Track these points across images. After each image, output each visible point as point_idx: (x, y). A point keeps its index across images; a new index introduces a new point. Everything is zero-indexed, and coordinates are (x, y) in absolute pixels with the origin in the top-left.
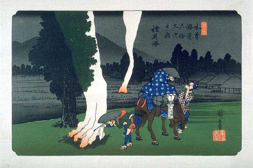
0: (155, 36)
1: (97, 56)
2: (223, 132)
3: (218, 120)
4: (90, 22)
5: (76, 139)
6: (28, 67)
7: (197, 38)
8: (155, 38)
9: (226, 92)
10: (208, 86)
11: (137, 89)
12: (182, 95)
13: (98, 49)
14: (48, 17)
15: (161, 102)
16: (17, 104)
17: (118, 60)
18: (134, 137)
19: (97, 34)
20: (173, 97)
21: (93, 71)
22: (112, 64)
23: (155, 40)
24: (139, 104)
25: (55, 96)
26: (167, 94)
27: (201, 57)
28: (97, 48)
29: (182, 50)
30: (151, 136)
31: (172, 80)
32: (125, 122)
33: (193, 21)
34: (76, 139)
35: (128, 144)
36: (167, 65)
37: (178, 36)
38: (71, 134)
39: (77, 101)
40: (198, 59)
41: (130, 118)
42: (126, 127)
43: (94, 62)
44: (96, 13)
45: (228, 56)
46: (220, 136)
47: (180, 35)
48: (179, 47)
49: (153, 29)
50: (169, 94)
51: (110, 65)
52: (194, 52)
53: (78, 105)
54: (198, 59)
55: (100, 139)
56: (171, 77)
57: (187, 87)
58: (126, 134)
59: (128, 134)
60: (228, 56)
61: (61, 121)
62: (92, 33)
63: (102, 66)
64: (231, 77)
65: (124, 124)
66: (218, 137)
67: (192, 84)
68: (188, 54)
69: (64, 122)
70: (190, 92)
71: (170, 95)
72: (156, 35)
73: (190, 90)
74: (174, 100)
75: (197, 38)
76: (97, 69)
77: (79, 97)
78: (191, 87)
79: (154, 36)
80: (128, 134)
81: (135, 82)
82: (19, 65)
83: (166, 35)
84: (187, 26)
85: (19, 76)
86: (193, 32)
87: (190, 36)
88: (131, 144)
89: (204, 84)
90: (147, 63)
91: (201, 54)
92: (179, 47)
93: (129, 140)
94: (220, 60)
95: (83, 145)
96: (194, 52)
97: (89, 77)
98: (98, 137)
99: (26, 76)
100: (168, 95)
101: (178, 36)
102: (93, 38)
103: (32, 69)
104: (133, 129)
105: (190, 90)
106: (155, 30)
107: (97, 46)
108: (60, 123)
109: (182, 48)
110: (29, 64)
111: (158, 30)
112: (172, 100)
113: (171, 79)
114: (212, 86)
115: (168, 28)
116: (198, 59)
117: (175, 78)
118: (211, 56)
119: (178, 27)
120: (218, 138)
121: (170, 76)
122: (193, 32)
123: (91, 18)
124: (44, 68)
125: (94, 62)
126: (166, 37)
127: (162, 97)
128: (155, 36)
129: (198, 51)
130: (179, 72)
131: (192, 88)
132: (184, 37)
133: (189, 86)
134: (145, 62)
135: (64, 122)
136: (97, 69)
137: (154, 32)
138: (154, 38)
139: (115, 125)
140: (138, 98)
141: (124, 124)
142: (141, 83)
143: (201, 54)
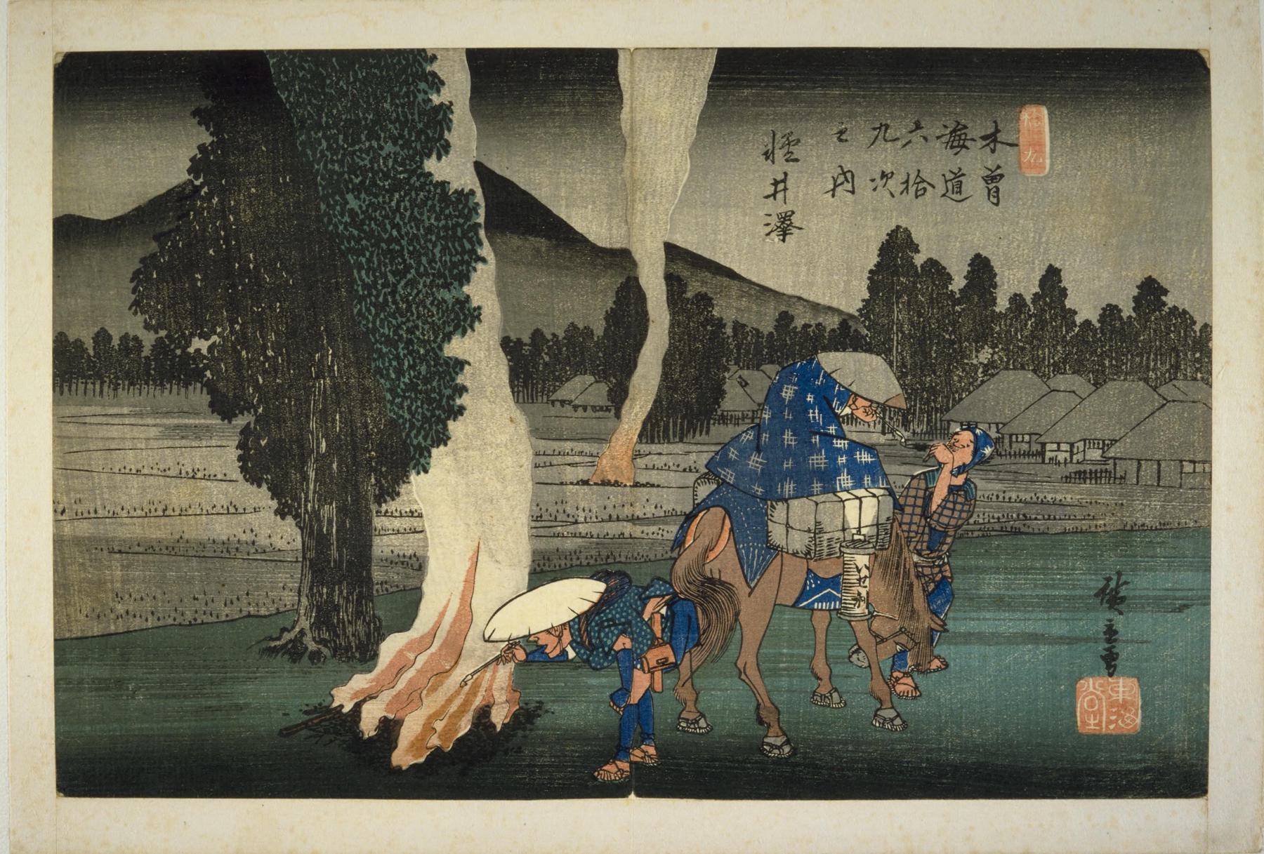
2: (1125, 688)
3: (1101, 626)
4: (446, 109)
5: (369, 724)
6: (130, 345)
8: (780, 196)
9: (1135, 464)
10: (1048, 447)
12: (910, 524)
14: (232, 88)
16: (78, 541)
20: (870, 506)
21: (460, 364)
22: (561, 335)
23: (779, 207)
27: (1017, 301)
28: (481, 244)
29: (919, 260)
34: (369, 724)
35: (637, 752)
36: (846, 337)
37: (894, 185)
38: (343, 698)
39: (378, 522)
40: (1002, 304)
44: (486, 64)
45: (1151, 291)
47: (907, 182)
48: (897, 247)
52: (981, 269)
53: (383, 546)
54: (1002, 304)
55: (494, 726)
60: (1151, 291)
63: (509, 346)
65: (617, 647)
68: (950, 278)
72: (784, 181)
74: (877, 525)
77: (392, 506)
78: (965, 456)
82: (84, 334)
85: (82, 387)
87: (956, 183)
91: (1016, 280)
95: (402, 757)
96: (981, 269)
98: (483, 714)
101: (894, 185)
102: (459, 193)
107: (482, 233)
110: (134, 325)
118: (1064, 293)
119: (897, 139)
120: (1101, 715)
123: (456, 88)
124: (210, 349)
125: (465, 317)
126: (839, 189)
127: (814, 507)
131: (968, 459)
132: (925, 189)
134: (730, 325)
136: (479, 354)
137: (773, 162)
141: (617, 647)
142: (707, 433)
143: (1016, 280)
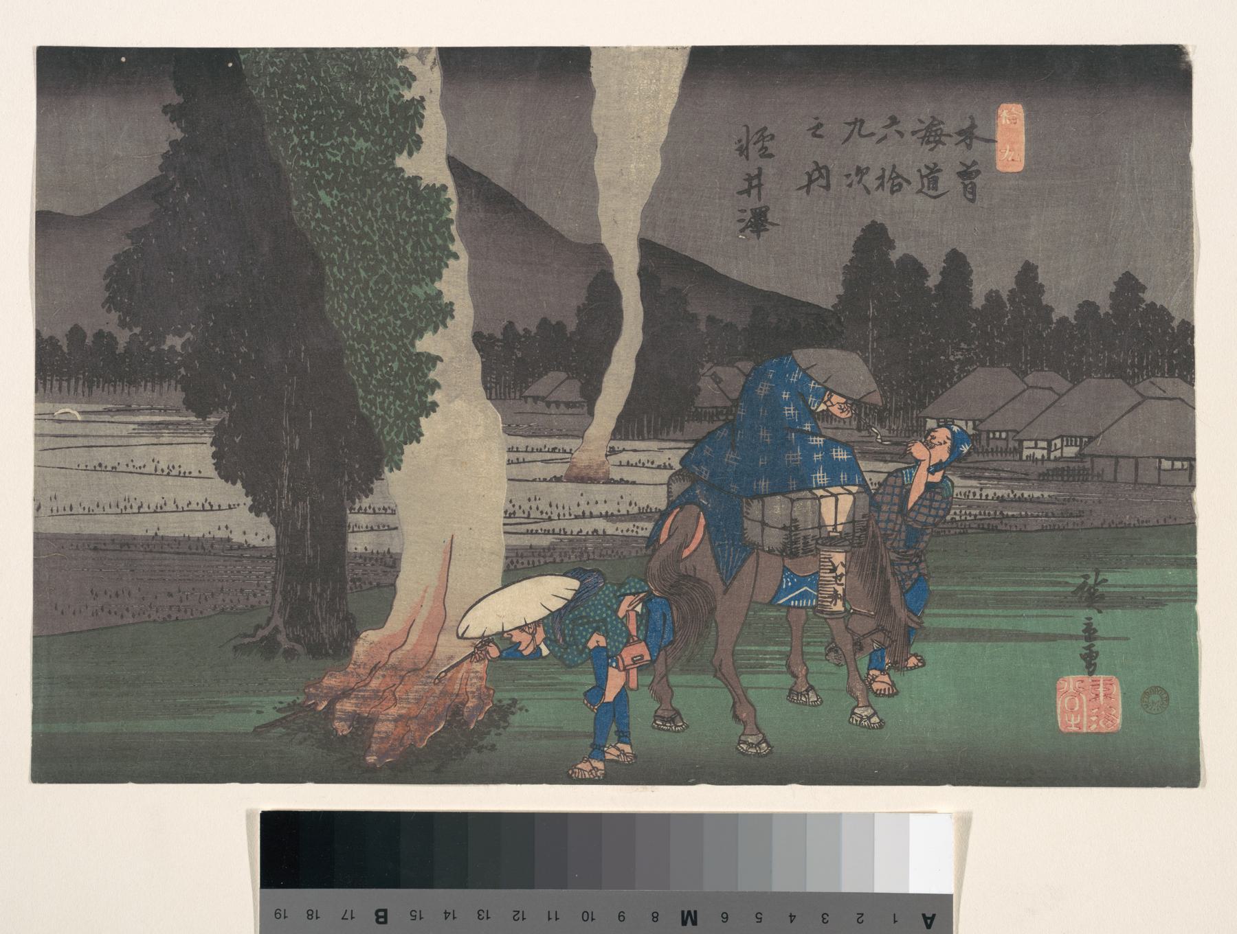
0: (754, 182)
1: (454, 284)
7: (971, 193)
8: (754, 192)
11: (661, 459)
13: (458, 246)
14: (203, 79)
15: (784, 528)
16: (56, 538)
17: (561, 301)
18: (642, 707)
19: (454, 165)
20: (846, 502)
23: (752, 202)
24: (670, 536)
25: (236, 493)
26: (817, 488)
28: (453, 240)
29: (895, 256)
30: (734, 706)
31: (843, 416)
32: (596, 637)
33: (952, 109)
41: (621, 614)
42: (602, 661)
43: (440, 313)
46: (1087, 706)
48: (874, 238)
49: (744, 142)
50: (823, 487)
51: (522, 333)
52: (957, 265)
53: (358, 543)
56: (836, 399)
57: (918, 450)
58: (604, 694)
59: (610, 696)
60: (1129, 286)
61: (268, 624)
62: (428, 164)
63: (479, 339)
64: (1145, 398)
66: (1081, 712)
67: (943, 434)
68: (85, 337)
69: (281, 628)
70: (932, 479)
71: (832, 495)
72: (759, 176)
73: (933, 470)
75: (971, 193)
76: (451, 348)
79: (749, 179)
80: (610, 696)
81: (649, 422)
83: (810, 175)
84: (919, 126)
86: (950, 155)
87: (932, 174)
88: (627, 749)
89: (1004, 435)
90: (234, 483)
91: (990, 279)
92: (874, 238)
93: (617, 732)
94: (1087, 309)
96: (957, 265)
97: (415, 392)
99: (90, 388)
100: (820, 492)
101: (870, 180)
103: (65, 349)
104: (640, 669)
105: (935, 465)
106: (753, 151)
108: (261, 633)
109: (891, 244)
111: (766, 148)
112: (842, 519)
113: (835, 410)
114: (1044, 444)
115: (820, 136)
116: (1102, 312)
117: (856, 404)
119: (872, 134)
121: (832, 391)
122: (950, 155)
123: (428, 83)
124: (184, 346)
125: (440, 313)
128: (754, 182)
129: (974, 261)
130: (876, 374)
132: (900, 185)
133: (929, 446)
135: (281, 628)
136: (451, 348)
138: (748, 191)
139: (545, 651)
140: (663, 506)
142: (682, 430)
143: (990, 279)
